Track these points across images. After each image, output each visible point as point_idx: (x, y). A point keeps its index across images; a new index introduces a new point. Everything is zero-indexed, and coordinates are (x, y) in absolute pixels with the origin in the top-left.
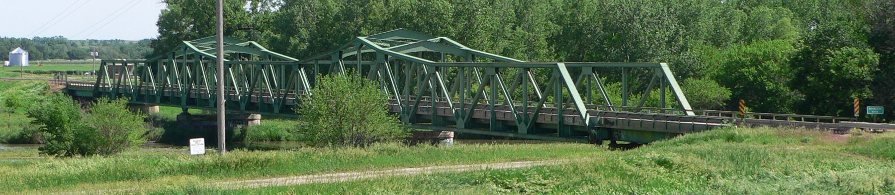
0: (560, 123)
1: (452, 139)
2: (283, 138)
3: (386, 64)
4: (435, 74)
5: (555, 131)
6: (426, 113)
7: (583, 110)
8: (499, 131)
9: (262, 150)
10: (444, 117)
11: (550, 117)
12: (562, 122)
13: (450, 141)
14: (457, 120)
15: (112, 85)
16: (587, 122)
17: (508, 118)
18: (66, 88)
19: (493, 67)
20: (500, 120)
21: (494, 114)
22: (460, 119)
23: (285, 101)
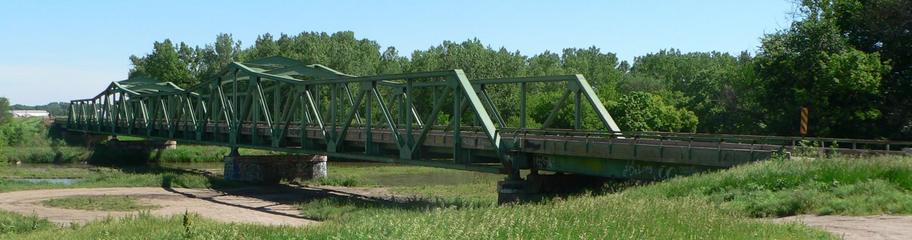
0: (456, 145)
1: (325, 163)
2: (192, 160)
3: (258, 86)
4: (305, 93)
5: (451, 156)
6: (296, 136)
7: (491, 128)
8: (376, 155)
9: (415, 200)
10: (314, 140)
11: (313, 133)
12: (459, 145)
13: (323, 164)
14: (328, 143)
15: (147, 121)
16: (498, 143)
17: (387, 140)
19: (369, 81)
20: (376, 143)
21: (370, 135)
22: (331, 142)
23: (178, 127)
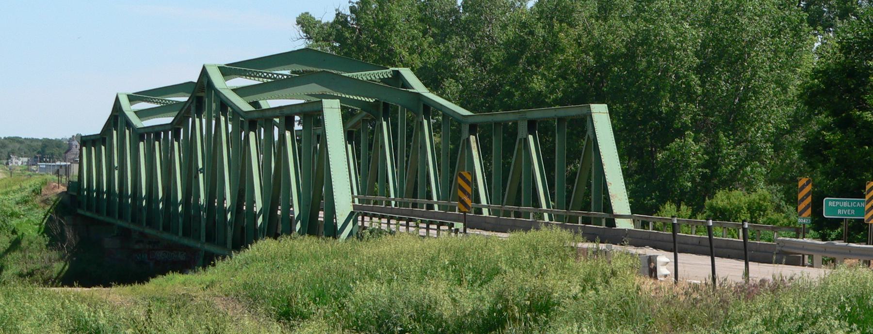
18: (66, 192)
